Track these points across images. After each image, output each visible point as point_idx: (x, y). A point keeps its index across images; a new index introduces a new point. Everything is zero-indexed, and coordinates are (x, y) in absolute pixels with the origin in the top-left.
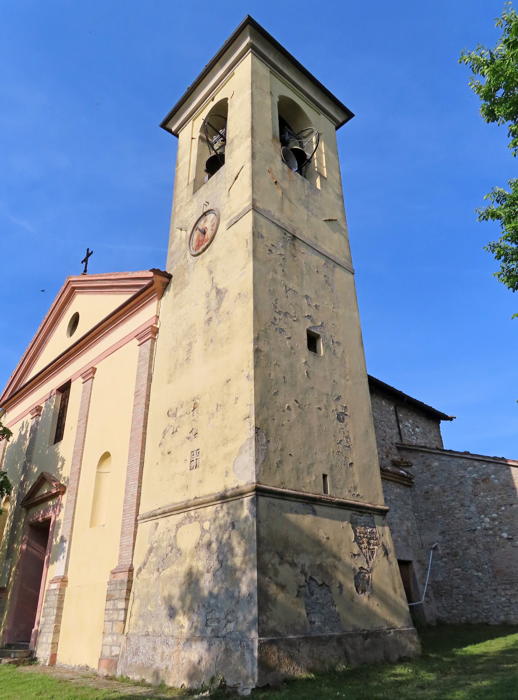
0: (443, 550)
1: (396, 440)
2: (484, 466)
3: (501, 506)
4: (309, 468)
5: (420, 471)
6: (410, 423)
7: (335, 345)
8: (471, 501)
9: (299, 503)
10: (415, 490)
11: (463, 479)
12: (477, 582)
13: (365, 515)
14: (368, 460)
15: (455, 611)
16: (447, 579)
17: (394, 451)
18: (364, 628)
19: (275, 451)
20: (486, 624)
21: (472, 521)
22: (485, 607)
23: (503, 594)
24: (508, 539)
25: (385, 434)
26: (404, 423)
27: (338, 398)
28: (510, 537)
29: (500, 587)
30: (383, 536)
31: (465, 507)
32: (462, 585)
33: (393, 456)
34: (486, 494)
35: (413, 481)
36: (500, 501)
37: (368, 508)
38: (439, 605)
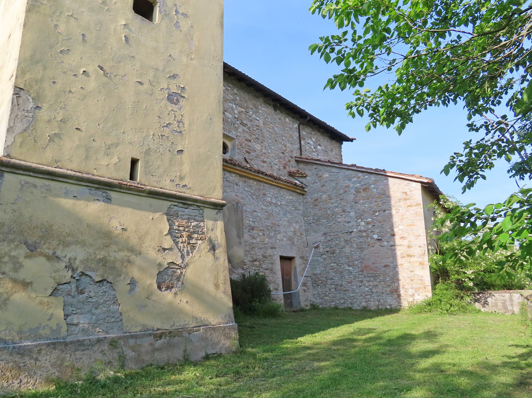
0: (324, 248)
1: (296, 154)
2: (366, 177)
3: (376, 211)
4: (109, 148)
5: (313, 182)
6: (312, 141)
7: (180, 16)
8: (352, 207)
9: (81, 187)
10: (306, 198)
11: (347, 189)
12: (348, 275)
13: (192, 208)
14: (207, 150)
15: (327, 298)
16: (324, 272)
17: (293, 163)
18: (159, 327)
19: (49, 121)
20: (350, 308)
21: (350, 224)
22: (352, 295)
23: (367, 284)
24: (378, 240)
25: (285, 148)
26: (307, 141)
27: (174, 76)
28: (380, 238)
29: (365, 279)
30: (212, 230)
31: (346, 212)
32: (335, 277)
33: (291, 167)
34: (365, 201)
35: (306, 190)
36: (375, 207)
37: (196, 201)
38: (316, 292)
